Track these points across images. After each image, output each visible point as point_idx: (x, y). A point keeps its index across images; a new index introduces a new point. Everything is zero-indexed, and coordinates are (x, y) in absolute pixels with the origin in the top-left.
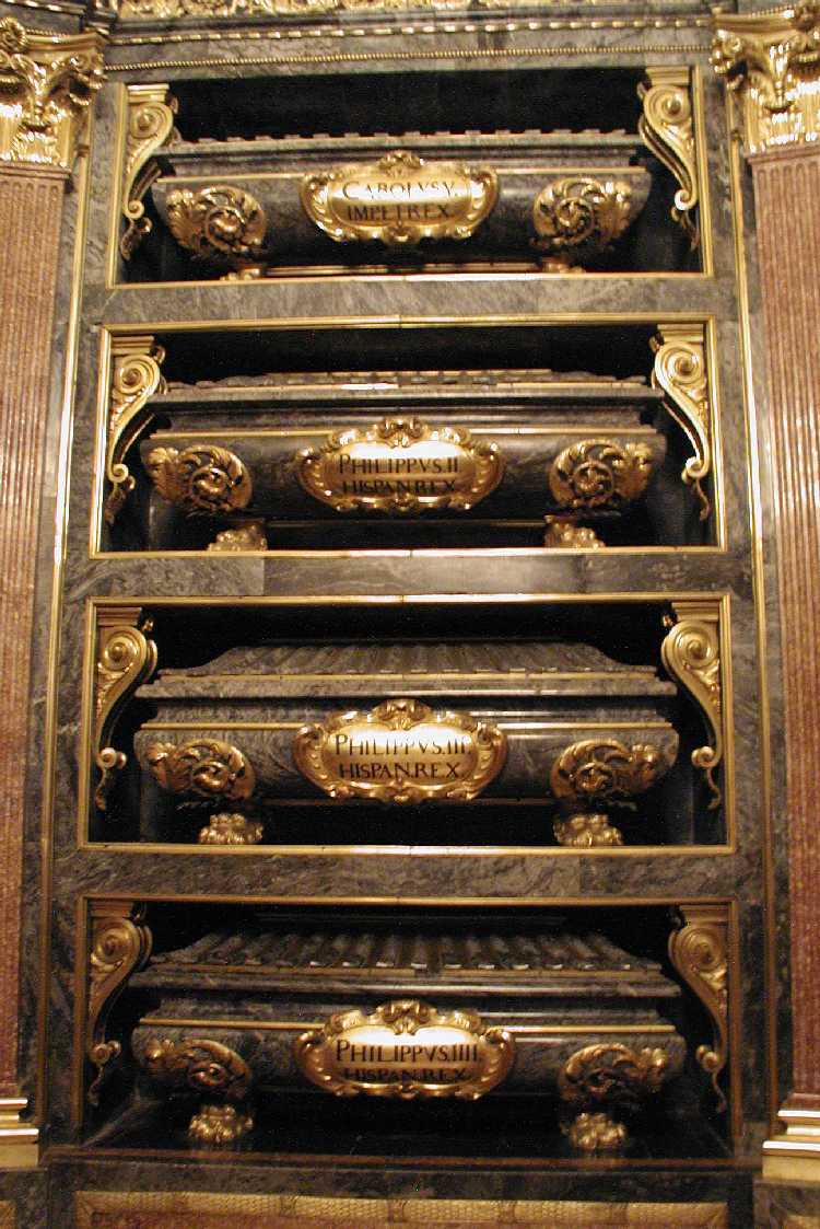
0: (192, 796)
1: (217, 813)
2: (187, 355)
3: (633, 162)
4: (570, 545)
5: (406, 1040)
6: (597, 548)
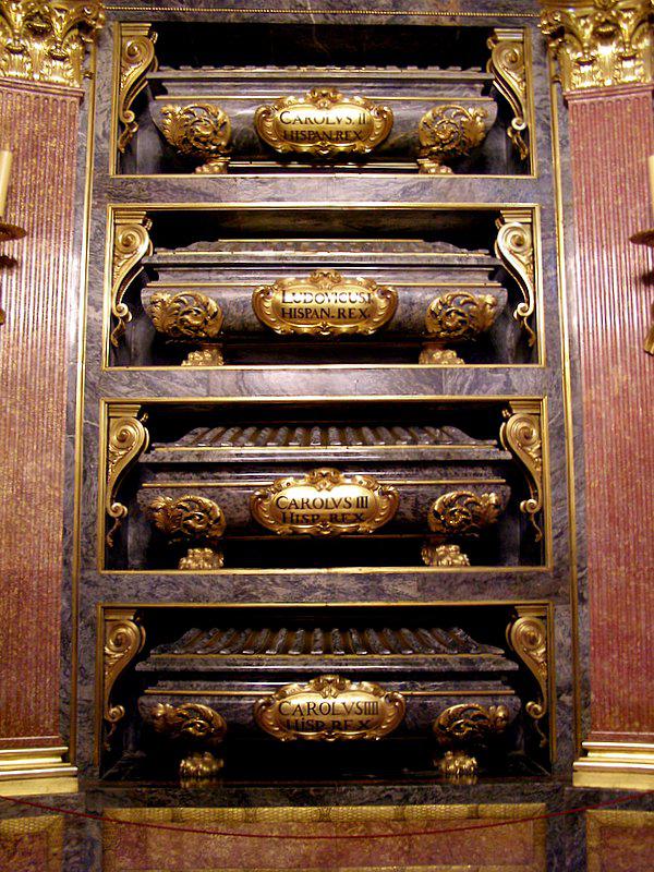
0: (179, 534)
1: (193, 548)
2: (172, 229)
3: (491, 277)
4: (438, 362)
5: (325, 495)
6: (460, 364)
